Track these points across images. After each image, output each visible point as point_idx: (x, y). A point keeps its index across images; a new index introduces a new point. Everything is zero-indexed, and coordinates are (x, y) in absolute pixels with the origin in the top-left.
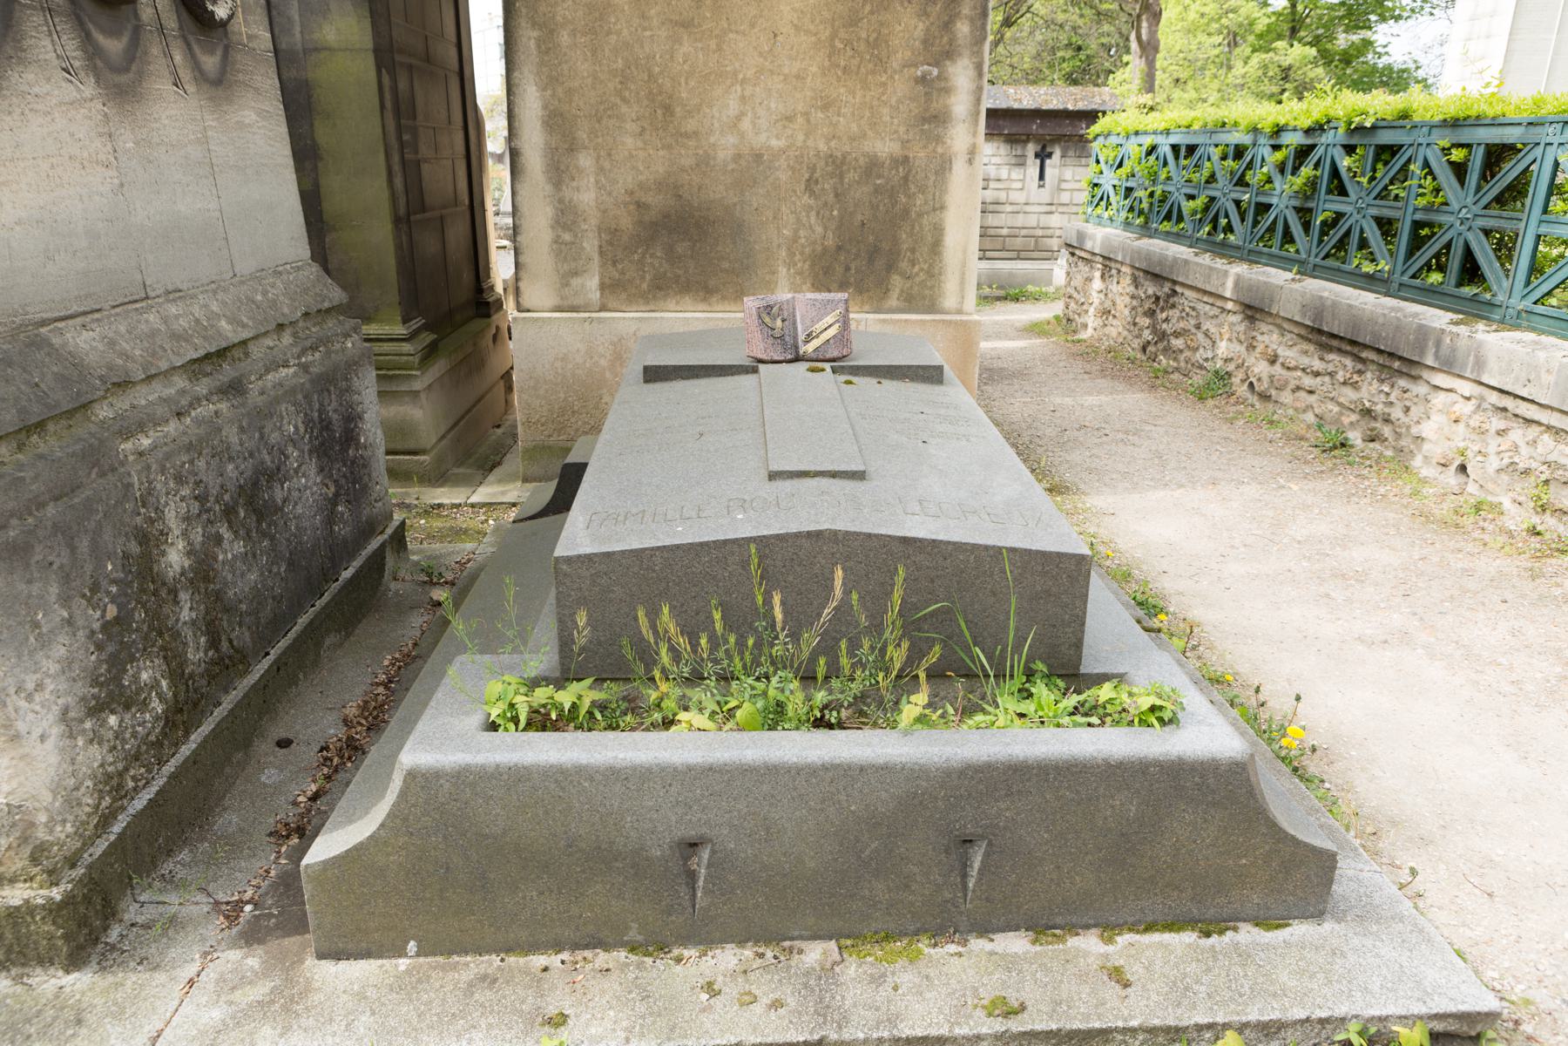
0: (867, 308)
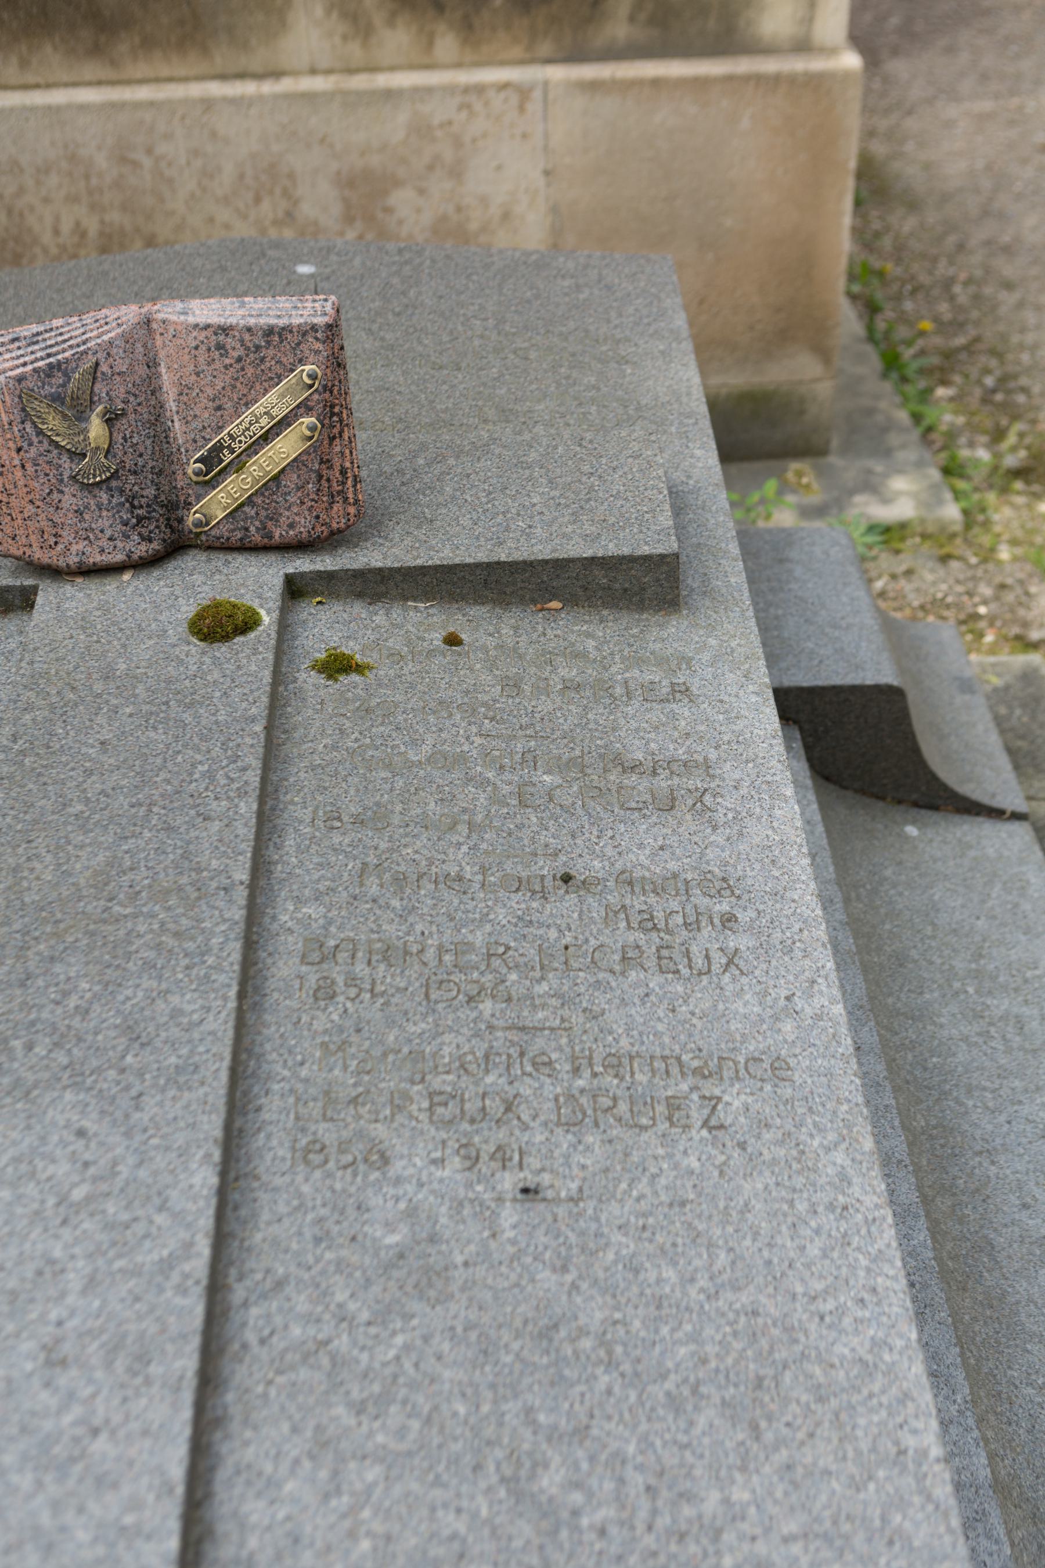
0: (545, 48)
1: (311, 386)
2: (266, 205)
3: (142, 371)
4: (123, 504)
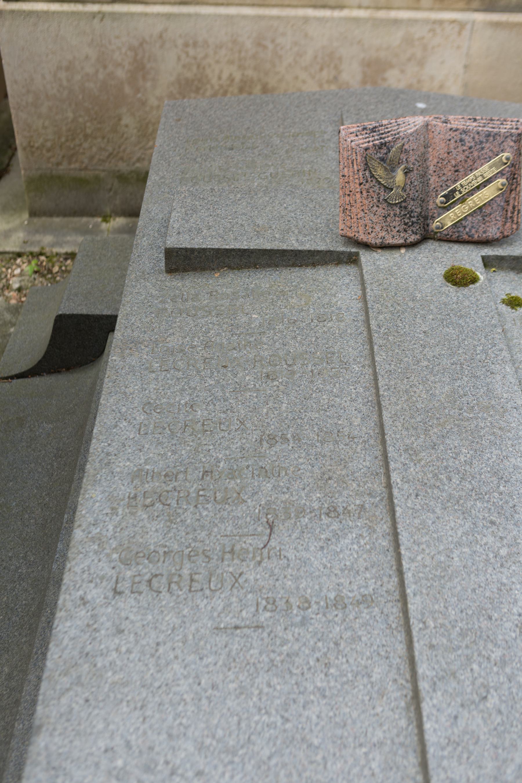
1: (506, 164)
2: (325, 73)
3: (422, 149)
4: (406, 215)
